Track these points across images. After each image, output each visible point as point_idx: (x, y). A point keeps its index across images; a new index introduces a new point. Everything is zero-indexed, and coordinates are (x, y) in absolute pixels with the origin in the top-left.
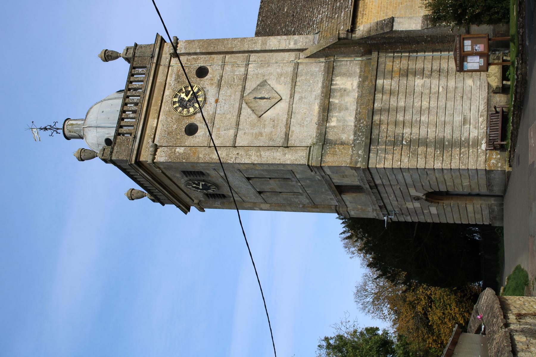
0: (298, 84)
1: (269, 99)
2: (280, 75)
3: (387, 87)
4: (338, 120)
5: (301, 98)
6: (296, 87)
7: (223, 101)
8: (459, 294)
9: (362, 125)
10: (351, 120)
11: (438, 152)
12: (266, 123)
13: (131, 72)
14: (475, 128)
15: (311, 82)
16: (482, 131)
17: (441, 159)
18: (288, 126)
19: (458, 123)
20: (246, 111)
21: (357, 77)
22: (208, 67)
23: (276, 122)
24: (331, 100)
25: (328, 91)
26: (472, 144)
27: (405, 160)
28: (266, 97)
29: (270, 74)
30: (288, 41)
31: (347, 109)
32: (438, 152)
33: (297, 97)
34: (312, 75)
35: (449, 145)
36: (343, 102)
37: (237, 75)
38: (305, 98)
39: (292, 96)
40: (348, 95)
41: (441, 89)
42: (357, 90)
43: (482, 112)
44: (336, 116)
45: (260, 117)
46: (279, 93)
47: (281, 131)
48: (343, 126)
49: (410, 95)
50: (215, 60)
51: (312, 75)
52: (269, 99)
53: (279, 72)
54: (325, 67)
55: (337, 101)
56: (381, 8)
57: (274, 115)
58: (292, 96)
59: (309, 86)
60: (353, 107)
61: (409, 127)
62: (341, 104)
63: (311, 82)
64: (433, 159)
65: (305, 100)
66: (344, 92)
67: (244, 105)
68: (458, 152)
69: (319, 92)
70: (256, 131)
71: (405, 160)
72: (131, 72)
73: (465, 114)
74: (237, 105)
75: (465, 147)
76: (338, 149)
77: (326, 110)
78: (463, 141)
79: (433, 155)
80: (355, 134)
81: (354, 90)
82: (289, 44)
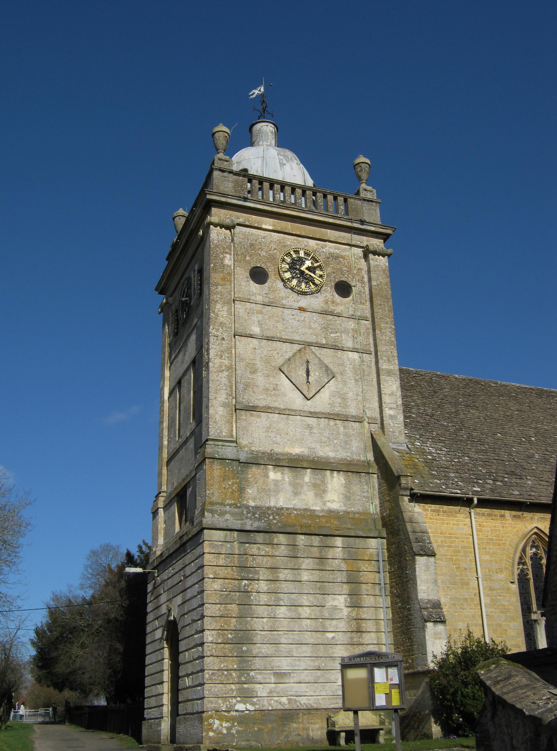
0: (332, 423)
3: (330, 553)
4: (278, 481)
6: (326, 420)
7: (302, 319)
9: (271, 517)
10: (282, 500)
11: (230, 636)
12: (271, 379)
14: (271, 692)
15: (335, 441)
16: (266, 703)
17: (220, 641)
18: (268, 410)
19: (277, 664)
20: (289, 350)
21: (344, 508)
23: (273, 392)
24: (308, 471)
25: (320, 466)
26: (244, 688)
27: (217, 585)
28: (310, 377)
30: (395, 406)
31: (296, 494)
32: (230, 636)
33: (312, 421)
34: (345, 442)
35: (242, 652)
36: (305, 488)
37: (341, 337)
40: (316, 495)
41: (330, 635)
42: (326, 508)
43: (296, 701)
44: (283, 479)
46: (317, 395)
49: (319, 589)
51: (345, 442)
55: (307, 479)
56: (449, 538)
57: (283, 389)
59: (329, 438)
60: (297, 503)
61: (269, 589)
62: (302, 486)
64: (218, 628)
65: (307, 434)
66: (320, 490)
67: (296, 347)
68: (230, 667)
70: (259, 364)
71: (217, 585)
73: (292, 675)
74: (297, 338)
75: (239, 677)
77: (295, 464)
78: (248, 674)
79: (226, 627)
80: (257, 508)
81: (324, 503)
82: (391, 408)
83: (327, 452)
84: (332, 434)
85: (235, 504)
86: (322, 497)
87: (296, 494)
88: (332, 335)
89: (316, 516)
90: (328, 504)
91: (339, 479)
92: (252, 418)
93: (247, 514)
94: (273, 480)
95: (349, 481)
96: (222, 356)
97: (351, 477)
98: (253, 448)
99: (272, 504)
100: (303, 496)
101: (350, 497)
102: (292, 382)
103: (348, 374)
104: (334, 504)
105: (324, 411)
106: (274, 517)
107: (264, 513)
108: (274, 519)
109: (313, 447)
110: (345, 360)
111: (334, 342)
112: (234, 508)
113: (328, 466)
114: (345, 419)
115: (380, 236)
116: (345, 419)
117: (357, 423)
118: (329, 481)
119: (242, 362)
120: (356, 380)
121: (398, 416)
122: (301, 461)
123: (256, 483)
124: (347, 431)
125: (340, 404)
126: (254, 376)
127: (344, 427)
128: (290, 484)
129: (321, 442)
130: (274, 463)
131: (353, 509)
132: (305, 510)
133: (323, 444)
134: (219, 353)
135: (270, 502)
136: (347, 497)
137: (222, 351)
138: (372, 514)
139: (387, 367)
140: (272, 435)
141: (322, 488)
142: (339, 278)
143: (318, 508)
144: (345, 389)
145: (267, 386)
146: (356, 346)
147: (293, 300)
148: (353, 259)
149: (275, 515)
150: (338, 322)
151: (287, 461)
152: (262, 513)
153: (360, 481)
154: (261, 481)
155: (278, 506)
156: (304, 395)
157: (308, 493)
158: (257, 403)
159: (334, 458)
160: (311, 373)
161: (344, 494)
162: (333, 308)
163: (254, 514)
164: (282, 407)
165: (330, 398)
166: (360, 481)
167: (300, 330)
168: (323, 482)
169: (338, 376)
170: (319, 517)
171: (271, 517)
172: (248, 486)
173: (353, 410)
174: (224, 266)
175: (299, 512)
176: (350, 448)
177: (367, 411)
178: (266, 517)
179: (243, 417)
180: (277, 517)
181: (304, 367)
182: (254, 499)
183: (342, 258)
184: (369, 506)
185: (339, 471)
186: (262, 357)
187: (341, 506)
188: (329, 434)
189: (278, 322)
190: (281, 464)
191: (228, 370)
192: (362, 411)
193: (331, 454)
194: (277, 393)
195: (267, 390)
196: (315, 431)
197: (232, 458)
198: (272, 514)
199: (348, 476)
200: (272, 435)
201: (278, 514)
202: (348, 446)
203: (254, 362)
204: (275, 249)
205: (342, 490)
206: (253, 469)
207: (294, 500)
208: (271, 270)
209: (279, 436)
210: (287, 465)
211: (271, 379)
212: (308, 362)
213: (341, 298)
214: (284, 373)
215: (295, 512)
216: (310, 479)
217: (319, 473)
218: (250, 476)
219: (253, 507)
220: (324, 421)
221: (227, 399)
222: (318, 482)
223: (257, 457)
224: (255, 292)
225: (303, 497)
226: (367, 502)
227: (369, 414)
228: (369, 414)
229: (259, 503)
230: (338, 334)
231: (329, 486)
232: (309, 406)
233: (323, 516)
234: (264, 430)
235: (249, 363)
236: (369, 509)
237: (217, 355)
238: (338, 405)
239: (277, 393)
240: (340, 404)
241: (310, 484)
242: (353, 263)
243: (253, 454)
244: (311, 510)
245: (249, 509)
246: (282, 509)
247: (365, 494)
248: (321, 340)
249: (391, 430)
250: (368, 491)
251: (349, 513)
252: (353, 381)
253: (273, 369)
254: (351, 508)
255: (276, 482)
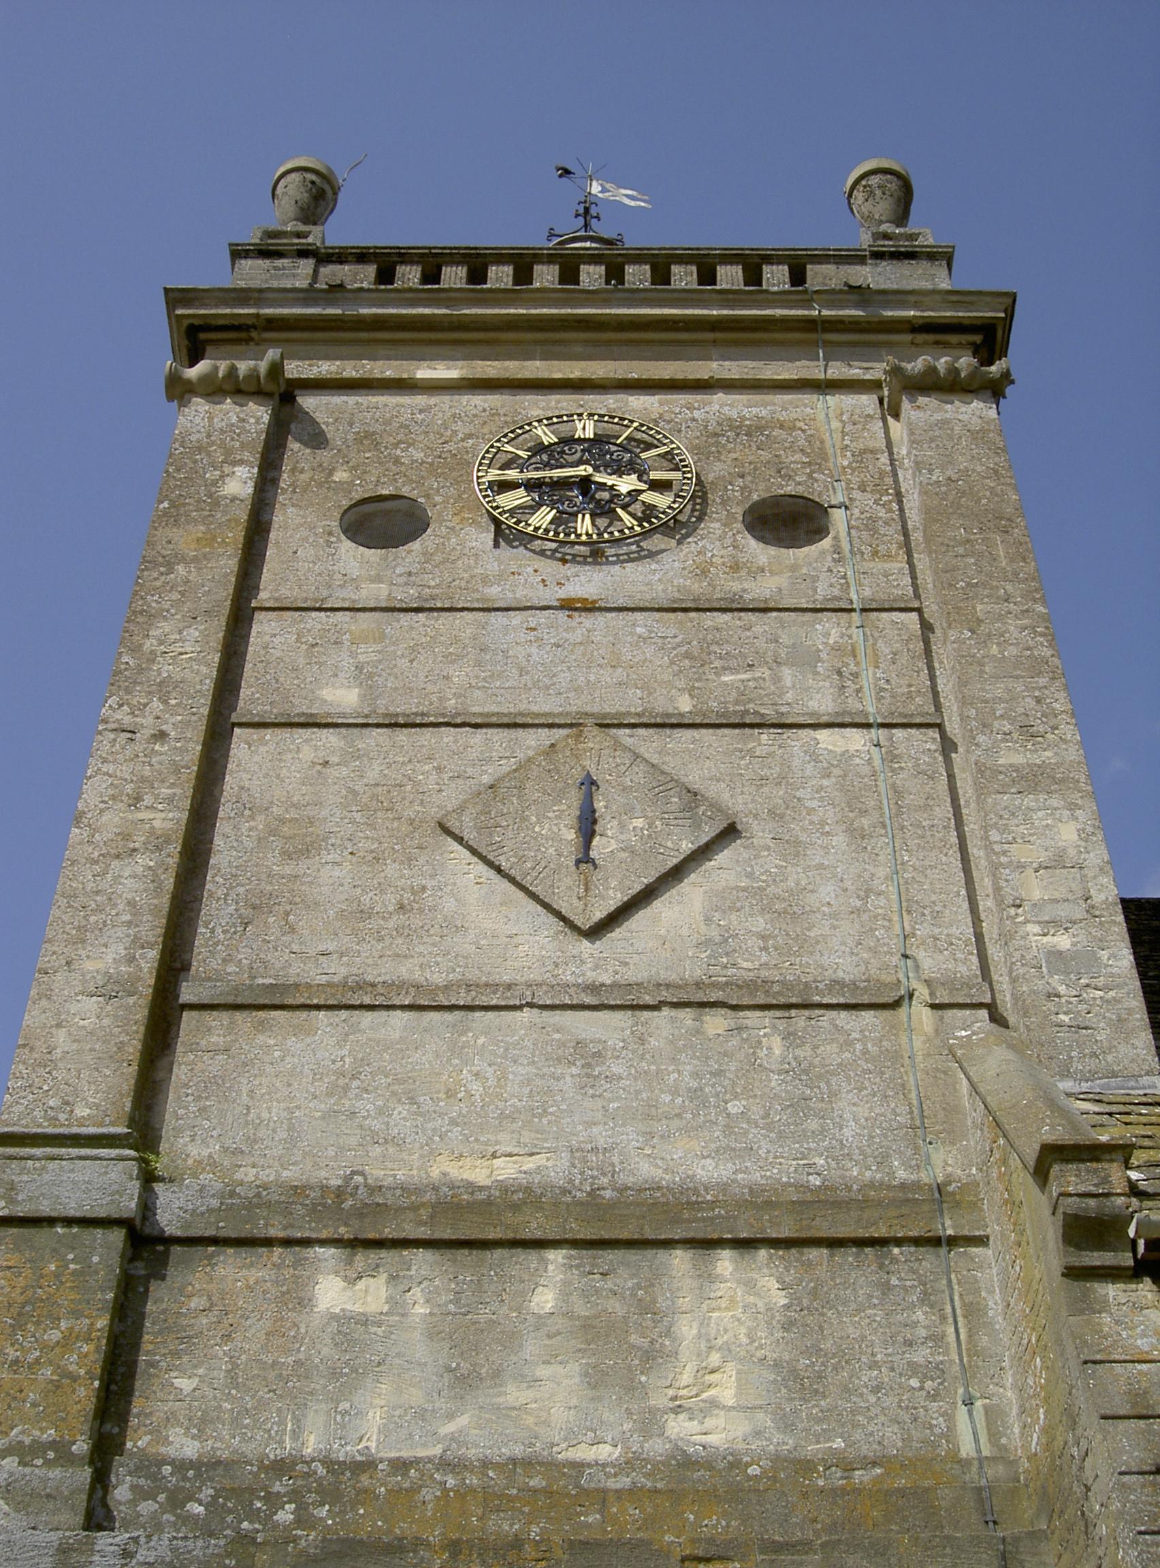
0: (716, 1023)
1: (585, 859)
2: (789, 911)
4: (364, 1321)
5: (588, 1056)
6: (686, 1015)
7: (578, 635)
8: (322, 1471)
9: (285, 1515)
10: (374, 1424)
12: (391, 869)
13: (768, 259)
15: (734, 1107)
20: (493, 754)
21: (781, 1442)
22: (826, 543)
24: (556, 1256)
25: (624, 1230)
29: (793, 849)
30: (1079, 912)
31: (463, 1382)
33: (607, 1028)
34: (799, 1106)
36: (531, 1347)
37: (777, 679)
38: (589, 1080)
39: (634, 1002)
40: (596, 1379)
42: (656, 1448)
44: (397, 1306)
45: (448, 832)
47: (314, 953)
48: (302, 1369)
50: (878, 566)
51: (799, 1106)
52: (585, 859)
53: (811, 900)
54: (872, 1185)
55: (545, 1300)
57: (449, 905)
58: (634, 1002)
59: (696, 1094)
60: (466, 1430)
62: (511, 1340)
63: (734, 1107)
66: (624, 1354)
69: (645, 1170)
72: (768, 259)
74: (544, 705)
76: (66, 1343)
77: (474, 1234)
80: (206, 1467)
81: (650, 1423)
83: (695, 1162)
84: (718, 1073)
85: (53, 1445)
86: (632, 1388)
87: (463, 1382)
88: (726, 679)
89: (586, 1492)
90: (679, 1428)
91: (750, 1285)
92: (261, 1039)
93: (133, 1503)
94: (334, 1317)
95: (814, 1293)
96: (138, 799)
97: (822, 1272)
98: (248, 1174)
99: (311, 1445)
100: (510, 1388)
101: (820, 1376)
102: (499, 870)
103: (811, 811)
104: (710, 1423)
105: (673, 977)
106: (301, 1508)
107: (243, 1494)
108: (303, 1519)
109: (601, 1143)
110: (796, 762)
111: (737, 703)
112: (48, 1463)
113: (676, 1221)
114: (791, 1003)
115: (954, 338)
116: (791, 1003)
117: (868, 1016)
118: (684, 1302)
119: (252, 818)
120: (857, 835)
121: (1104, 954)
122: (515, 1207)
123: (227, 1337)
124: (805, 1052)
125: (764, 938)
126: (303, 866)
127: (788, 1036)
128: (433, 1334)
129: (648, 1117)
130: (344, 1232)
131: (838, 1443)
132: (528, 1464)
133: (660, 1127)
134: (129, 788)
135: (295, 1435)
136: (801, 1380)
137: (143, 780)
138: (965, 1464)
139: (1018, 759)
140: (366, 1105)
141: (634, 1338)
142: (768, 489)
143: (605, 1452)
144: (795, 875)
145: (366, 899)
146: (853, 704)
147: (533, 576)
148: (835, 424)
149: (311, 1498)
150: (757, 629)
151: (424, 1214)
152: (235, 1492)
153: (886, 1288)
154: (256, 1329)
155: (346, 1451)
156: (564, 919)
157: (542, 1371)
158: (298, 971)
159: (724, 1187)
160: (608, 826)
161: (777, 1365)
162: (736, 586)
163: (177, 1500)
164: (438, 978)
165: (708, 920)
166: (886, 1288)
167: (564, 678)
168: (647, 1308)
169: (759, 832)
170: (602, 1497)
171: (285, 1515)
172: (176, 1354)
173: (839, 958)
174: (217, 504)
175: (473, 1480)
176: (823, 1130)
177: (921, 954)
178: (253, 1515)
179: (216, 1039)
180: (323, 1512)
181: (571, 803)
182: (201, 1425)
183: (782, 427)
184: (950, 1418)
185: (745, 1244)
186: (354, 793)
187: (758, 1434)
188: (696, 1075)
189: (450, 659)
190: (388, 1232)
191: (158, 848)
192: (895, 960)
193: (709, 1171)
194: (417, 922)
195: (365, 914)
196: (617, 1069)
197: (86, 1211)
198: (295, 1495)
199: (809, 1264)
200: (366, 1105)
201: (330, 1494)
202: (813, 1124)
203: (310, 812)
204: (470, 436)
205: (769, 1344)
206: (221, 1271)
207: (451, 1416)
208: (438, 501)
209: (401, 1111)
210: (423, 1233)
211: (391, 869)
212: (590, 784)
213: (772, 551)
214: (460, 840)
215: (451, 1482)
216: (565, 1293)
217: (625, 1270)
218: (194, 1303)
219: (181, 1466)
220: (673, 1020)
221: (131, 960)
222: (617, 1307)
223: (258, 1201)
224: (355, 574)
225: (514, 1394)
226: (934, 1397)
227: (929, 963)
228: (929, 963)
229: (225, 1442)
230: (763, 672)
231: (687, 1329)
232: (594, 962)
233: (633, 1493)
234: (321, 1087)
235: (282, 821)
236: (950, 1434)
237: (113, 798)
238: (754, 943)
239: (417, 922)
240: (764, 938)
241: (560, 1323)
242: (837, 436)
243: (232, 1194)
244: (551, 1466)
245: (156, 1477)
246: (367, 1465)
247: (921, 1355)
248: (672, 699)
249: (1065, 1018)
250: (937, 1339)
251: (806, 1466)
252: (840, 840)
253: (405, 828)
254: (827, 1435)
255: (349, 1326)
